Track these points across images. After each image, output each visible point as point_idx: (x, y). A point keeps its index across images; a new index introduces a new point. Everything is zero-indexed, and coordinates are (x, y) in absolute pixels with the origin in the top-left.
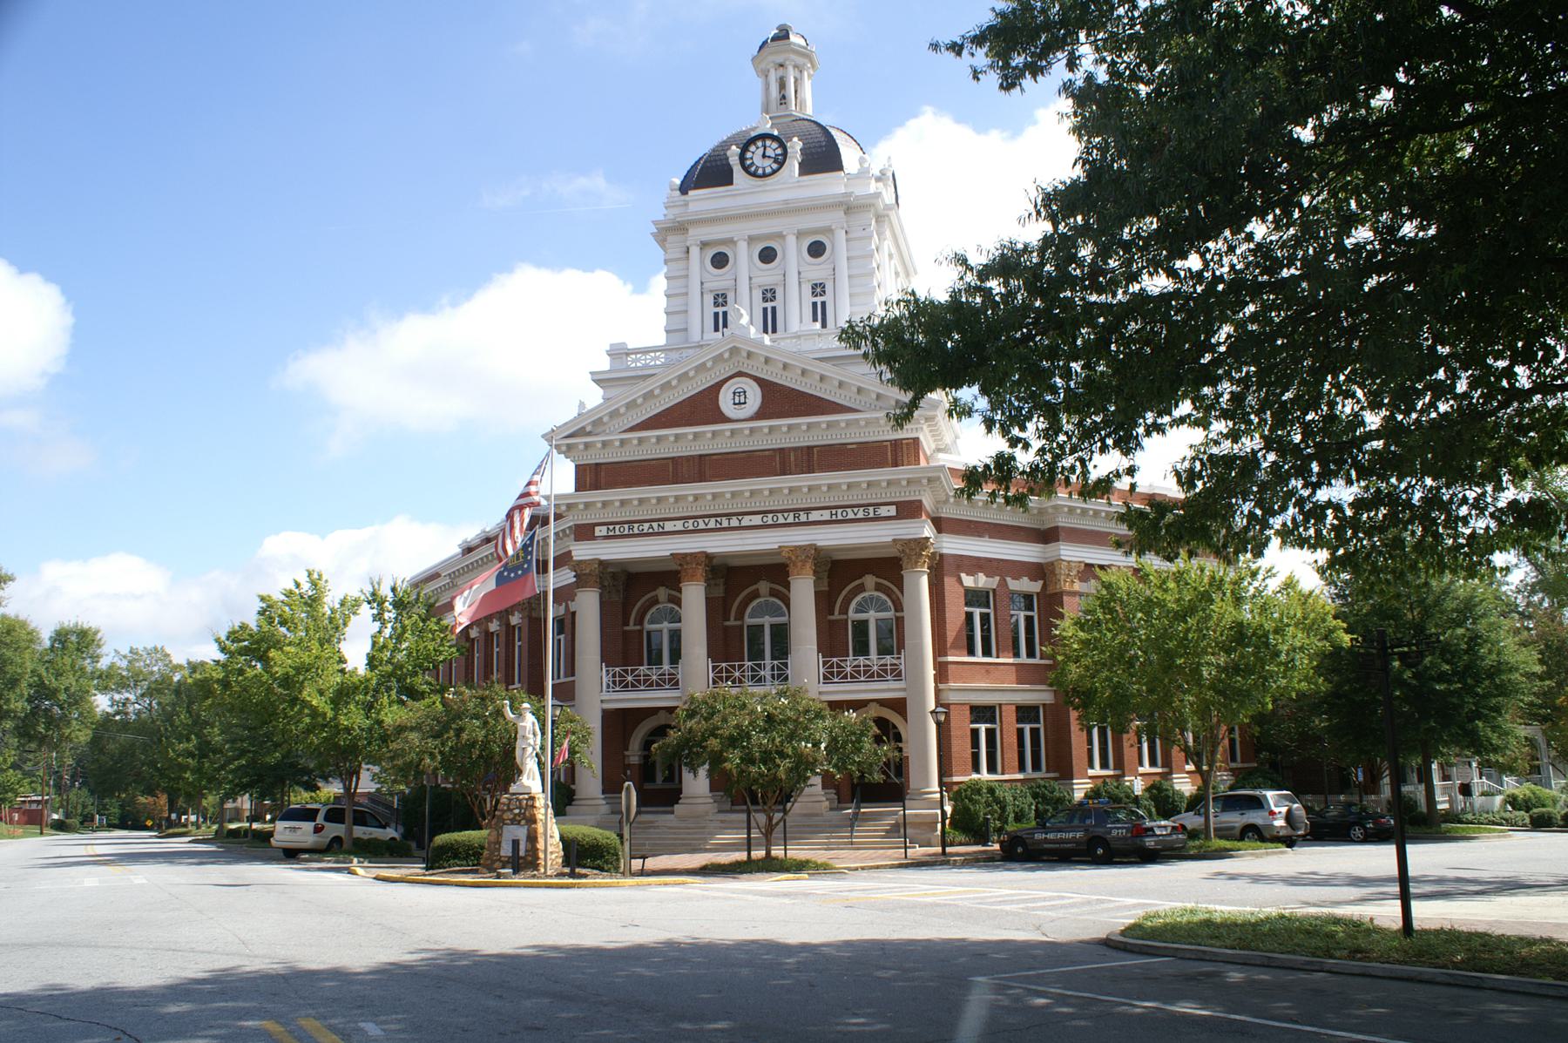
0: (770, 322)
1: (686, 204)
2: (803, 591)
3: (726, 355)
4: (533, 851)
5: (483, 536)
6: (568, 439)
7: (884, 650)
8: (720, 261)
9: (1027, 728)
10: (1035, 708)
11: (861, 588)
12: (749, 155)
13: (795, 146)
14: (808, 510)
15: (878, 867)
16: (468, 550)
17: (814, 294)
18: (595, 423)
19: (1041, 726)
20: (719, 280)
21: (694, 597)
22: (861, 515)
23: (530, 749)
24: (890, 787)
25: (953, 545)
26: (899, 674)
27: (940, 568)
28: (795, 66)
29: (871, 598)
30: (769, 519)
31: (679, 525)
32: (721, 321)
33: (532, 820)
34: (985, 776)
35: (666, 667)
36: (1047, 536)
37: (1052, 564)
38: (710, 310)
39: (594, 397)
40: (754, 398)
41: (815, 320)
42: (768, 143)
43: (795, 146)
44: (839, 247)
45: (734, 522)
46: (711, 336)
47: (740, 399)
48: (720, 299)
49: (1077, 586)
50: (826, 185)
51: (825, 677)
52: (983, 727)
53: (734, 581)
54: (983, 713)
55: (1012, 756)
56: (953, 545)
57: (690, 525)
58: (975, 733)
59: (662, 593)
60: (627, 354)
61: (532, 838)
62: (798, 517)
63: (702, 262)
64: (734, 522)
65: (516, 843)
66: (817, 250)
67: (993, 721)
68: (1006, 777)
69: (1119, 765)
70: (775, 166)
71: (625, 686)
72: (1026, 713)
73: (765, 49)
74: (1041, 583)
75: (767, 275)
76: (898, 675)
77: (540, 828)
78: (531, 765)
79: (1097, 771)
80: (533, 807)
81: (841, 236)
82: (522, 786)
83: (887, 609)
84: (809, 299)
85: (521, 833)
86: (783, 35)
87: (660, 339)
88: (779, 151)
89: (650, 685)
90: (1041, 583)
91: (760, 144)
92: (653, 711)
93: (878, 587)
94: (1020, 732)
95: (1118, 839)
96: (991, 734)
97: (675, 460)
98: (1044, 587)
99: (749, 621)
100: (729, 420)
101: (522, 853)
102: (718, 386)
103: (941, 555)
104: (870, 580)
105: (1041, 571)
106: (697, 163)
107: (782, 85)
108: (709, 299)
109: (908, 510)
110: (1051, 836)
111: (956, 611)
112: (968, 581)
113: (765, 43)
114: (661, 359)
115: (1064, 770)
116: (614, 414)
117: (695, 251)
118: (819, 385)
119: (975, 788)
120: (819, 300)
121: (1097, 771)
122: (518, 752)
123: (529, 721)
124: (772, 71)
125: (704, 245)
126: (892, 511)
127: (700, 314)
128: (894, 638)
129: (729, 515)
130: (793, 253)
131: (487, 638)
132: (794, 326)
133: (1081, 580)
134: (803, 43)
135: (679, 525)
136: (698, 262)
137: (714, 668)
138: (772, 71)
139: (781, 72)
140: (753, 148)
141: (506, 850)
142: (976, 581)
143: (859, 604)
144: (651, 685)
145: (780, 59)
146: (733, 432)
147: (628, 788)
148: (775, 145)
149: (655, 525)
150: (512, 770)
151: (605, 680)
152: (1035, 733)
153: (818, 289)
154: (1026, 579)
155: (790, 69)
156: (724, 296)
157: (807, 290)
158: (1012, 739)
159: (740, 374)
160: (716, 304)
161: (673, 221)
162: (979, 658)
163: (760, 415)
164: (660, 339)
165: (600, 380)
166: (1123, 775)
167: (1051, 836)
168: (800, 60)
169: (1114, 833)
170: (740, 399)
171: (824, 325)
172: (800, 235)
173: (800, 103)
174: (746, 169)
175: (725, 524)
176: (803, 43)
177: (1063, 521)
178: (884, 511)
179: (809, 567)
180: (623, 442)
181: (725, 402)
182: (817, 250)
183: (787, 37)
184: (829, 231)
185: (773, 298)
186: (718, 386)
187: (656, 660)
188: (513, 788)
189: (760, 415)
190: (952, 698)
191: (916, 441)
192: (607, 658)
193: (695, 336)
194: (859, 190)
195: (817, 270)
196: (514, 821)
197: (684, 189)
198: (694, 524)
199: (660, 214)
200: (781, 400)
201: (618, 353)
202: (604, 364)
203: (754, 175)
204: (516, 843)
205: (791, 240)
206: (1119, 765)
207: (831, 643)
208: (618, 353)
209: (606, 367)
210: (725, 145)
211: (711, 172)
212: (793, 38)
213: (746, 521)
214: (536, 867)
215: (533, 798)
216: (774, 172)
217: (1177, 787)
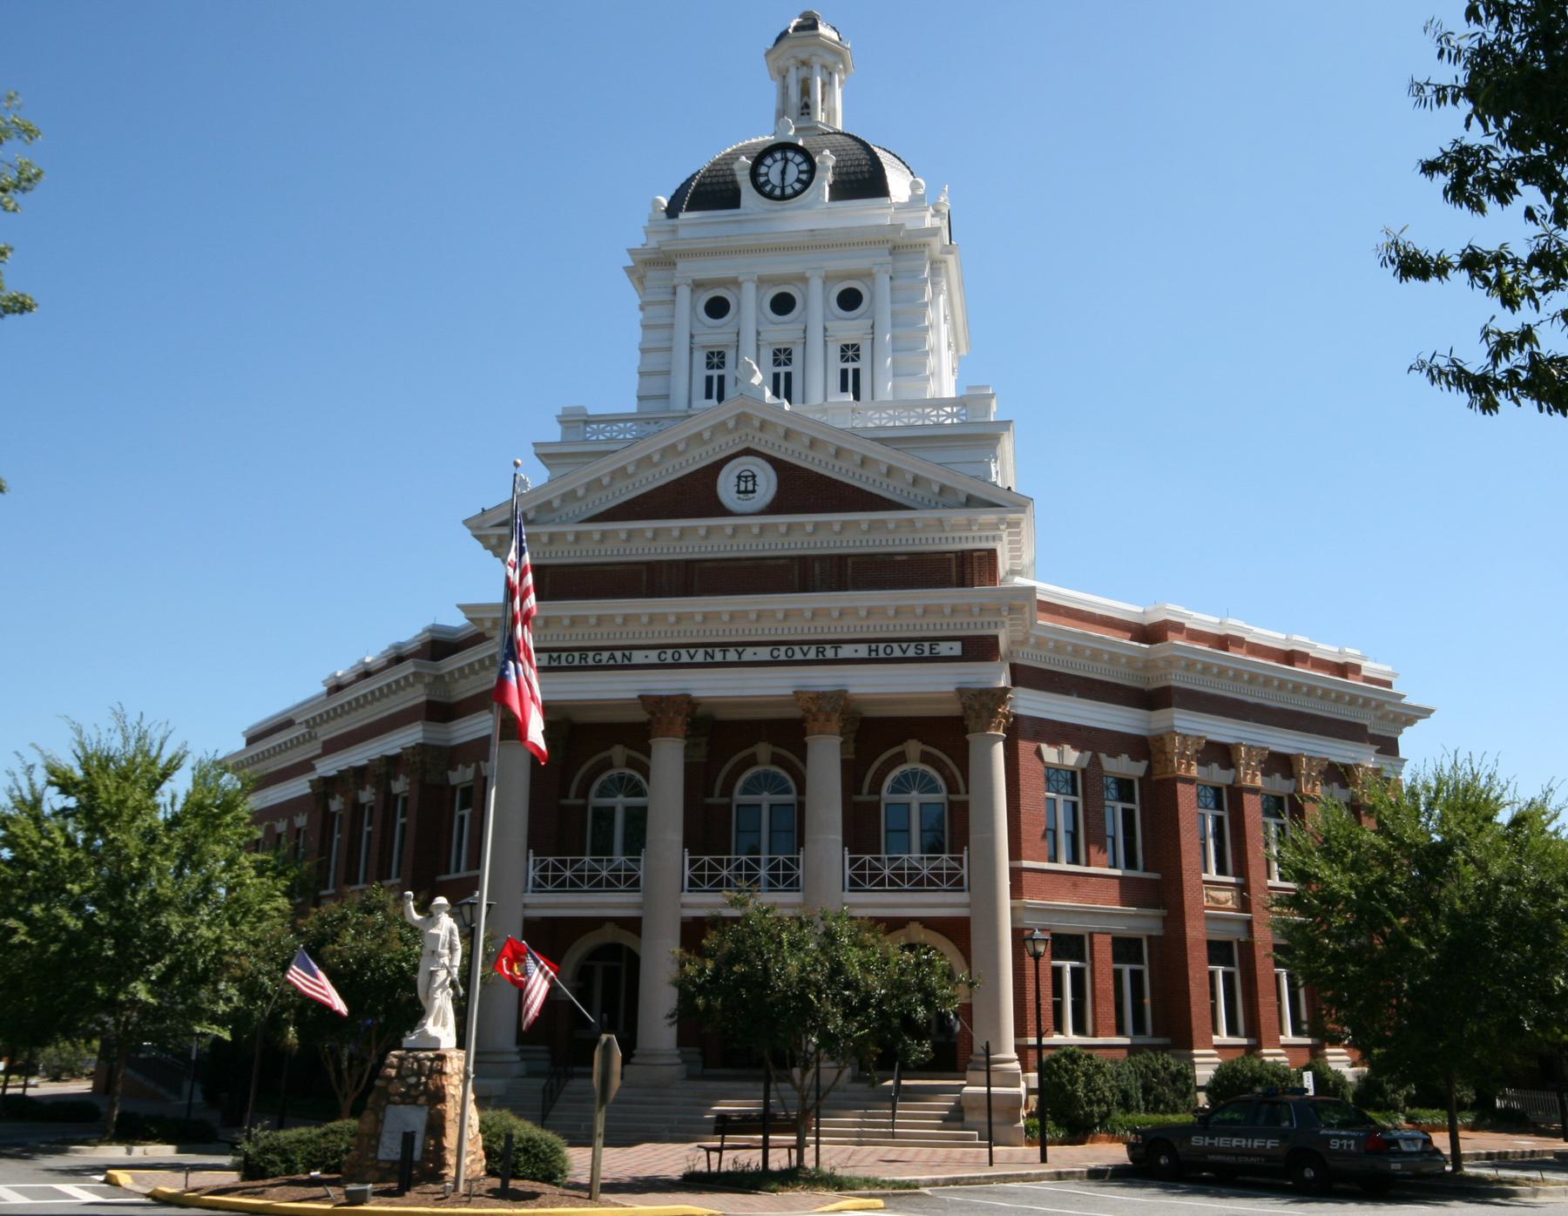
0: (783, 386)
1: (674, 231)
2: (826, 759)
3: (731, 424)
4: (437, 1155)
5: (361, 669)
6: (495, 531)
7: (933, 847)
8: (717, 308)
9: (1126, 969)
10: (1228, 944)
11: (901, 758)
12: (763, 170)
13: (827, 161)
14: (837, 643)
15: (956, 1181)
16: (336, 688)
17: (845, 358)
18: (539, 508)
19: (1145, 968)
20: (716, 333)
21: (669, 760)
22: (911, 653)
23: (442, 974)
24: (953, 1051)
25: (1030, 703)
26: (960, 882)
27: (1018, 730)
28: (824, 67)
29: (914, 773)
30: (782, 653)
31: (653, 656)
32: (716, 389)
33: (439, 1096)
34: (1069, 1038)
35: (619, 858)
36: (1153, 699)
37: (1160, 738)
38: (701, 372)
39: (536, 476)
40: (767, 485)
41: (844, 388)
42: (790, 155)
43: (827, 161)
44: (880, 298)
45: (732, 656)
46: (701, 403)
47: (746, 485)
48: (716, 359)
49: (1195, 771)
50: (861, 213)
51: (853, 883)
52: (1067, 966)
53: (719, 738)
54: (1068, 945)
55: (1107, 1009)
56: (1030, 703)
57: (668, 656)
58: (1212, 975)
59: (618, 753)
60: (587, 423)
61: (436, 1127)
62: (823, 652)
63: (693, 308)
64: (732, 656)
65: (408, 1139)
66: (850, 300)
67: (1081, 958)
68: (1099, 1041)
69: (1253, 1030)
70: (798, 186)
71: (561, 885)
72: (1125, 948)
73: (785, 44)
74: (1143, 765)
75: (782, 331)
76: (957, 884)
77: (451, 1110)
78: (443, 1002)
79: (1223, 1038)
80: (441, 1073)
81: (883, 284)
82: (425, 1034)
83: (936, 790)
84: (836, 365)
85: (415, 1118)
86: (809, 24)
87: (631, 406)
88: (804, 167)
89: (598, 885)
90: (1143, 765)
91: (778, 156)
92: (598, 922)
93: (926, 758)
94: (1118, 975)
95: (1339, 1153)
96: (1077, 974)
97: (650, 565)
98: (1149, 769)
99: (595, 801)
100: (726, 512)
101: (417, 1155)
102: (718, 466)
103: (1016, 717)
104: (913, 748)
105: (1140, 747)
106: (693, 177)
107: (806, 90)
108: (700, 358)
109: (980, 648)
110: (1221, 1142)
111: (1035, 793)
112: (1050, 754)
113: (784, 34)
114: (630, 431)
115: (1177, 1032)
116: (569, 497)
117: (684, 293)
118: (859, 471)
119: (1070, 1054)
120: (850, 366)
121: (1223, 1038)
122: (421, 978)
123: (446, 925)
124: (793, 71)
125: (698, 285)
126: (957, 649)
127: (686, 378)
128: (954, 830)
129: (724, 646)
130: (817, 303)
131: (375, 798)
132: (816, 397)
133: (1200, 763)
134: (834, 36)
135: (653, 656)
136: (688, 308)
137: (692, 863)
138: (793, 71)
139: (804, 72)
140: (769, 161)
141: (389, 1149)
142: (1061, 754)
143: (897, 781)
144: (599, 884)
145: (803, 56)
146: (736, 529)
147: (608, 1047)
148: (798, 159)
149: (618, 654)
150: (415, 1013)
151: (531, 873)
152: (1136, 977)
153: (850, 352)
154: (1125, 757)
155: (817, 68)
156: (721, 355)
157: (835, 353)
158: (1106, 985)
159: (748, 452)
160: (710, 366)
161: (657, 250)
162: (1063, 866)
163: (774, 508)
164: (631, 406)
165: (547, 455)
166: (1259, 1046)
167: (1221, 1142)
168: (829, 59)
169: (1335, 1144)
170: (746, 485)
171: (857, 397)
172: (828, 279)
173: (831, 114)
174: (759, 187)
175: (719, 657)
176: (834, 36)
177: (1177, 680)
178: (943, 649)
179: (835, 725)
180: (578, 536)
181: (726, 488)
182: (850, 300)
183: (814, 26)
184: (868, 275)
185: (788, 362)
186: (718, 466)
187: (603, 847)
188: (411, 1039)
189: (774, 508)
190: (1028, 922)
191: (992, 554)
192: (538, 841)
193: (680, 402)
194: (910, 222)
195: (850, 328)
196: (409, 1099)
197: (672, 211)
198: (673, 656)
199: (638, 240)
200: (803, 490)
201: (574, 421)
202: (554, 433)
203: (770, 196)
204: (408, 1139)
205: (816, 286)
206: (1253, 1030)
207: (861, 830)
208: (574, 421)
209: (558, 438)
210: (734, 156)
211: (711, 192)
212: (823, 30)
213: (749, 654)
214: (438, 1178)
215: (442, 1058)
216: (797, 194)
217: (1334, 1067)
